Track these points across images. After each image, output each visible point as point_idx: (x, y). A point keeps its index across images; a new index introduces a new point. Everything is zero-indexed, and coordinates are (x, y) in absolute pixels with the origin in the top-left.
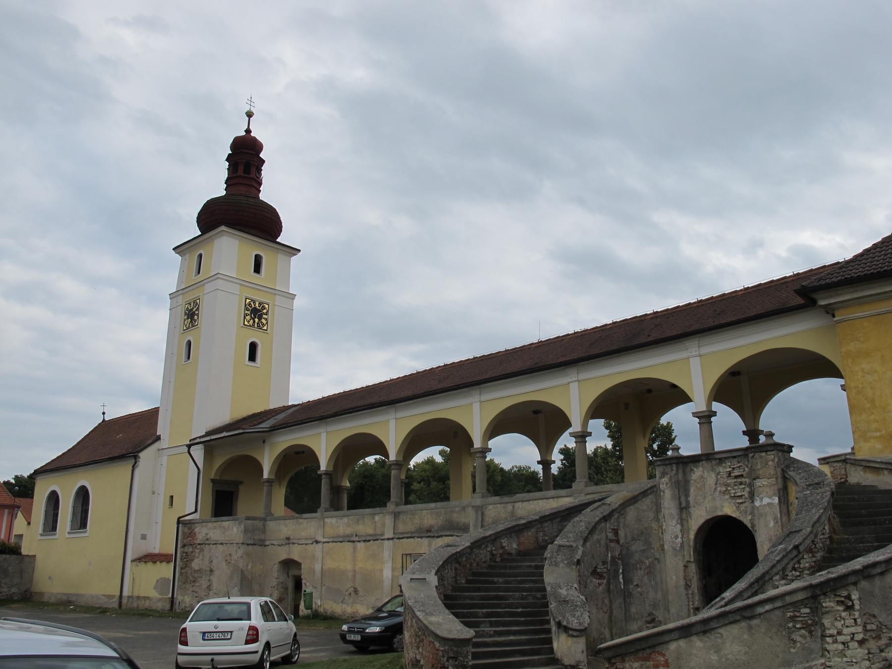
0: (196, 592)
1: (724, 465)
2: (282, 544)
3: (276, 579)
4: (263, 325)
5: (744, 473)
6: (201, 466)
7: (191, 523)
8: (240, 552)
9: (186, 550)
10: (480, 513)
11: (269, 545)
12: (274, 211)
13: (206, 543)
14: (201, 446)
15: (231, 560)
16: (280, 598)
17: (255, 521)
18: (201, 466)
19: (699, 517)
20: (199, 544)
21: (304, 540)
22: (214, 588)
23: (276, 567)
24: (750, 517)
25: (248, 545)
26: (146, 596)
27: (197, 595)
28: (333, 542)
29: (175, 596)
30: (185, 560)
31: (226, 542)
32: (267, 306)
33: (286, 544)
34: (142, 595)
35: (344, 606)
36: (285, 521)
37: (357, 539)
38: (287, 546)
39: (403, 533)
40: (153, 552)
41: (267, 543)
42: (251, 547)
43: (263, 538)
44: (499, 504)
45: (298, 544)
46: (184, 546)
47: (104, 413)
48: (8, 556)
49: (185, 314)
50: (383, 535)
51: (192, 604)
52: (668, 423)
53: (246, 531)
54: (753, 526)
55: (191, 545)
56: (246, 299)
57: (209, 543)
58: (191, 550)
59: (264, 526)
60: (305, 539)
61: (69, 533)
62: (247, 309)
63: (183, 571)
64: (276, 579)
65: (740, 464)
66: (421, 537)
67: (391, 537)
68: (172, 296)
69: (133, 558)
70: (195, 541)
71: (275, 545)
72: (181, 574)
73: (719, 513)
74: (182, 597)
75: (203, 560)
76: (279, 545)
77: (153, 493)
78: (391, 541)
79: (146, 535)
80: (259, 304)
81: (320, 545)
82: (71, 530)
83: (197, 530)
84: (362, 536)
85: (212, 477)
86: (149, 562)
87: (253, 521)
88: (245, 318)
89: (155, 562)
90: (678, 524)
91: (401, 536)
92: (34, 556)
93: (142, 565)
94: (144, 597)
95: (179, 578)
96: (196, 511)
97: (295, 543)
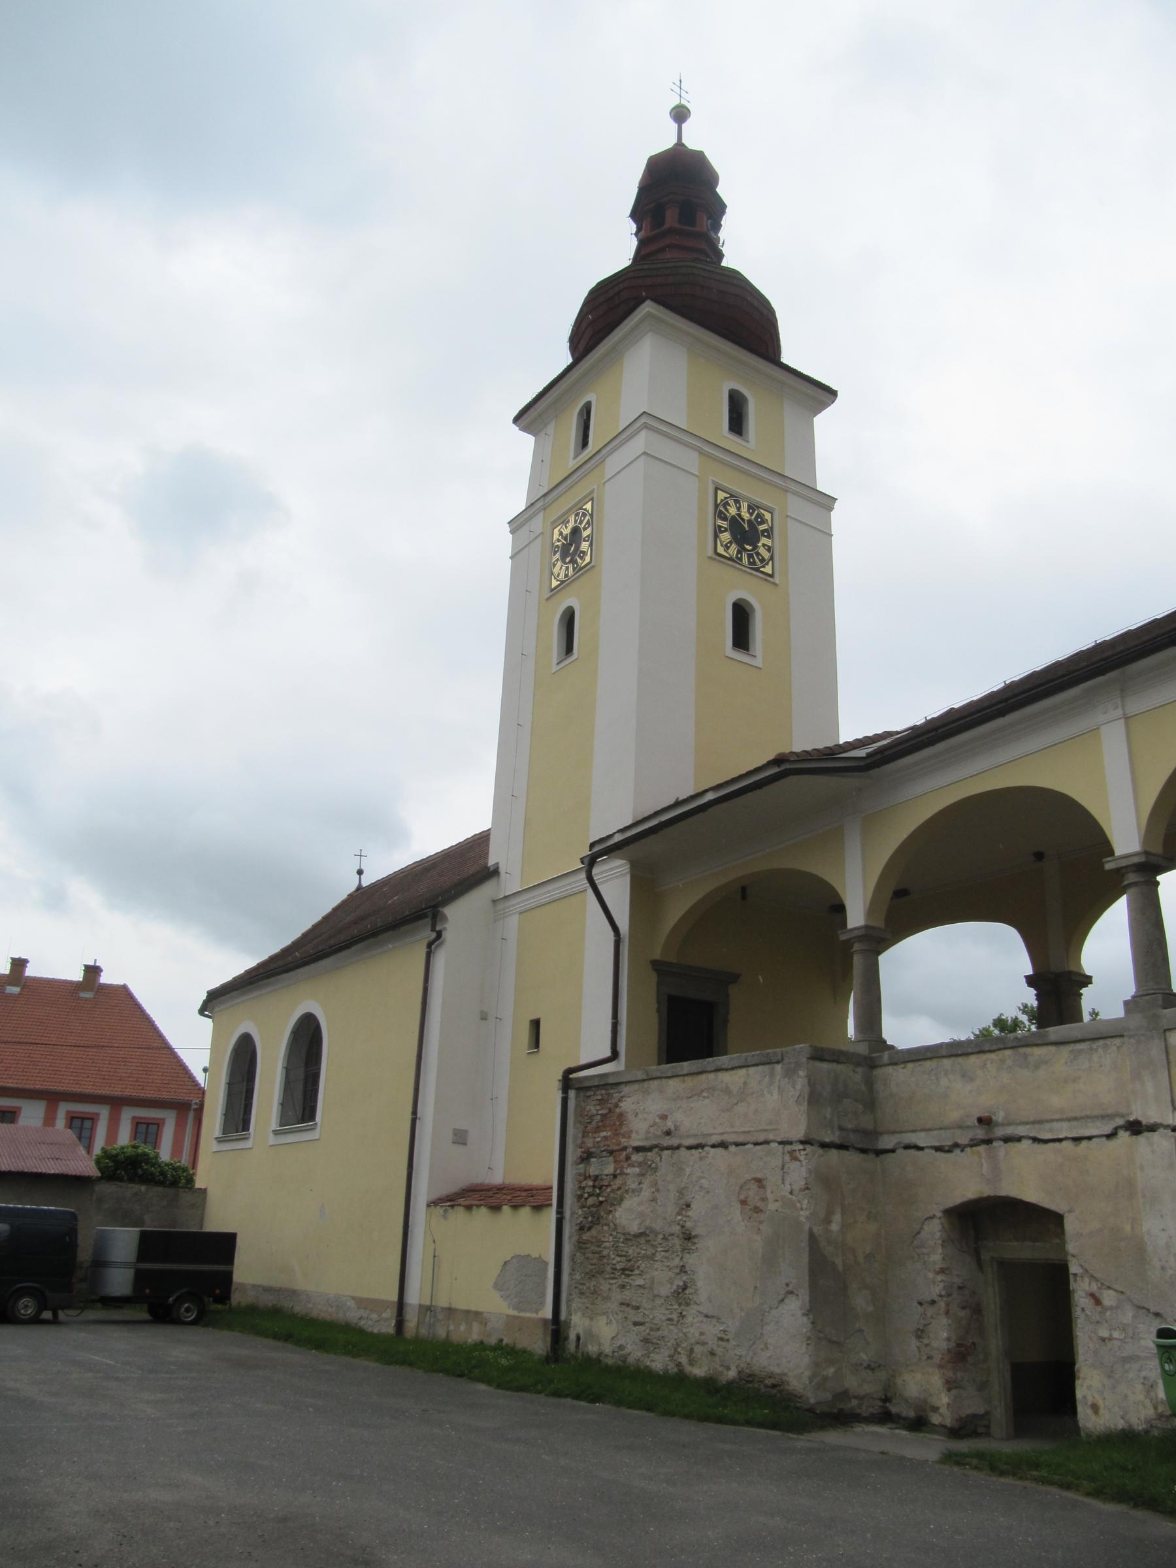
2: (956, 1145)
3: (942, 1271)
4: (762, 560)
6: (624, 924)
7: (607, 1085)
8: (798, 1174)
9: (594, 1168)
11: (893, 1151)
12: (765, 312)
15: (764, 1199)
16: (959, 1345)
17: (841, 1067)
18: (624, 924)
20: (638, 1149)
21: (1065, 1125)
22: (703, 1296)
23: (934, 1231)
25: (824, 1146)
26: (473, 1308)
27: (639, 1319)
30: (591, 1201)
31: (741, 1139)
32: (768, 516)
33: (974, 1143)
34: (462, 1304)
36: (960, 1060)
38: (982, 1149)
40: (487, 1181)
41: (887, 1142)
43: (870, 1127)
45: (1035, 1140)
46: (586, 1157)
47: (360, 872)
48: (143, 1188)
51: (621, 1347)
55: (611, 1153)
56: (716, 489)
58: (610, 1169)
59: (870, 1083)
61: (276, 1133)
63: (585, 1237)
64: (942, 1271)
68: (516, 525)
71: (921, 1149)
72: (581, 1245)
74: (587, 1322)
75: (654, 1200)
76: (938, 1149)
77: (484, 1017)
79: (466, 1131)
80: (749, 507)
82: (280, 1126)
83: (627, 1105)
85: (657, 954)
86: (478, 1206)
87: (834, 1066)
88: (716, 536)
89: (496, 1208)
92: (205, 1190)
93: (458, 1216)
94: (468, 1312)
95: (573, 1258)
96: (615, 1055)
97: (1019, 1139)
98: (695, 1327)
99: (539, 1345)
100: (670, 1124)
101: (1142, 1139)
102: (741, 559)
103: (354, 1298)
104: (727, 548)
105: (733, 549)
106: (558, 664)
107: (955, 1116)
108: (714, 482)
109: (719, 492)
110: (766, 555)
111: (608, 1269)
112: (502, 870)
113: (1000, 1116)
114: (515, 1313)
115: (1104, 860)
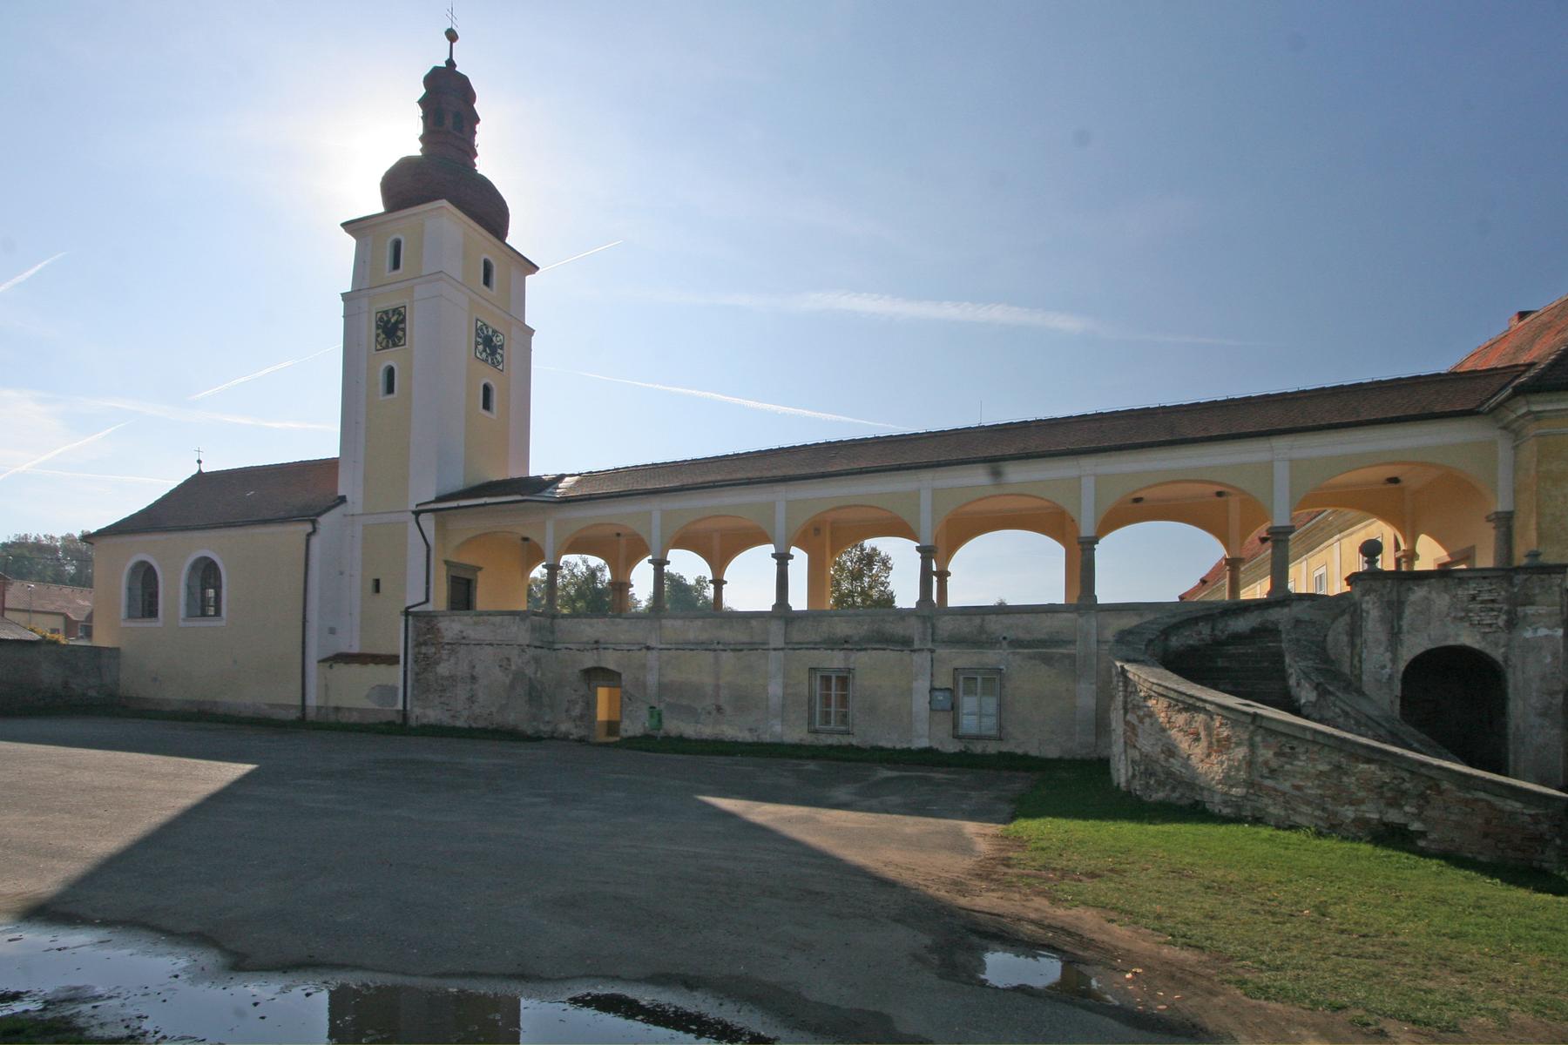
1: (1466, 586)
4: (498, 362)
5: (1500, 598)
10: (929, 625)
13: (461, 641)
14: (431, 516)
19: (1415, 645)
20: (448, 644)
24: (1503, 650)
25: (536, 647)
27: (449, 708)
28: (677, 649)
29: (408, 707)
35: (699, 726)
37: (721, 647)
38: (595, 651)
39: (800, 643)
41: (556, 646)
42: (539, 650)
44: (961, 615)
45: (614, 649)
49: (378, 327)
52: (669, 562)
53: (533, 629)
54: (1506, 659)
56: (477, 320)
58: (433, 650)
60: (627, 644)
62: (478, 335)
65: (1494, 587)
66: (832, 649)
67: (781, 647)
69: (321, 658)
70: (440, 640)
72: (417, 681)
73: (1451, 642)
78: (781, 653)
81: (655, 653)
84: (730, 644)
88: (476, 347)
90: (1388, 651)
91: (796, 647)
95: (413, 686)
96: (427, 600)
99: (399, 721)
100: (464, 634)
101: (649, 652)
103: (266, 704)
104: (481, 354)
105: (484, 355)
107: (585, 639)
109: (479, 322)
111: (432, 690)
112: (348, 498)
113: (602, 640)
114: (380, 708)
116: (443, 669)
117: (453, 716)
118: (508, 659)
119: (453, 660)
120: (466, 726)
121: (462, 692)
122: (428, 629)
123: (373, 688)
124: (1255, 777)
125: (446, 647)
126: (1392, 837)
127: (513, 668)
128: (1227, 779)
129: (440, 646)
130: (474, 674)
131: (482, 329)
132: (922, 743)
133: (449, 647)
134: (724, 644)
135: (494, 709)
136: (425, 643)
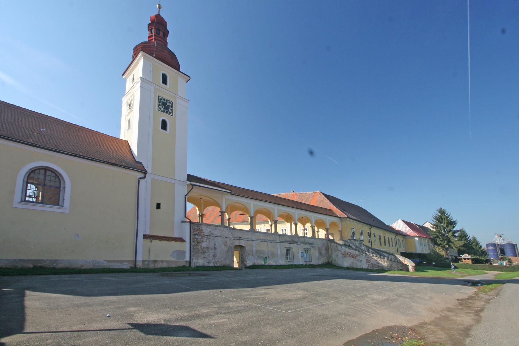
0: (206, 258)
4: (170, 112)
27: (207, 259)
28: (259, 241)
50: (369, 233)
57: (213, 235)
62: (159, 102)
88: (158, 106)
97: (242, 240)
98: (217, 259)
99: (187, 265)
101: (253, 241)
102: (164, 112)
104: (161, 109)
106: (128, 130)
108: (158, 94)
110: (171, 111)
111: (200, 252)
115: (316, 237)
116: (204, 245)
117: (208, 262)
118: (226, 242)
119: (208, 241)
120: (213, 265)
121: (211, 253)
122: (198, 229)
123: (174, 252)
124: (391, 265)
125: (205, 236)
126: (401, 270)
127: (228, 245)
128: (388, 266)
129: (203, 236)
130: (215, 247)
131: (161, 100)
132: (301, 263)
133: (207, 236)
134: (269, 240)
135: (222, 259)
136: (197, 234)
